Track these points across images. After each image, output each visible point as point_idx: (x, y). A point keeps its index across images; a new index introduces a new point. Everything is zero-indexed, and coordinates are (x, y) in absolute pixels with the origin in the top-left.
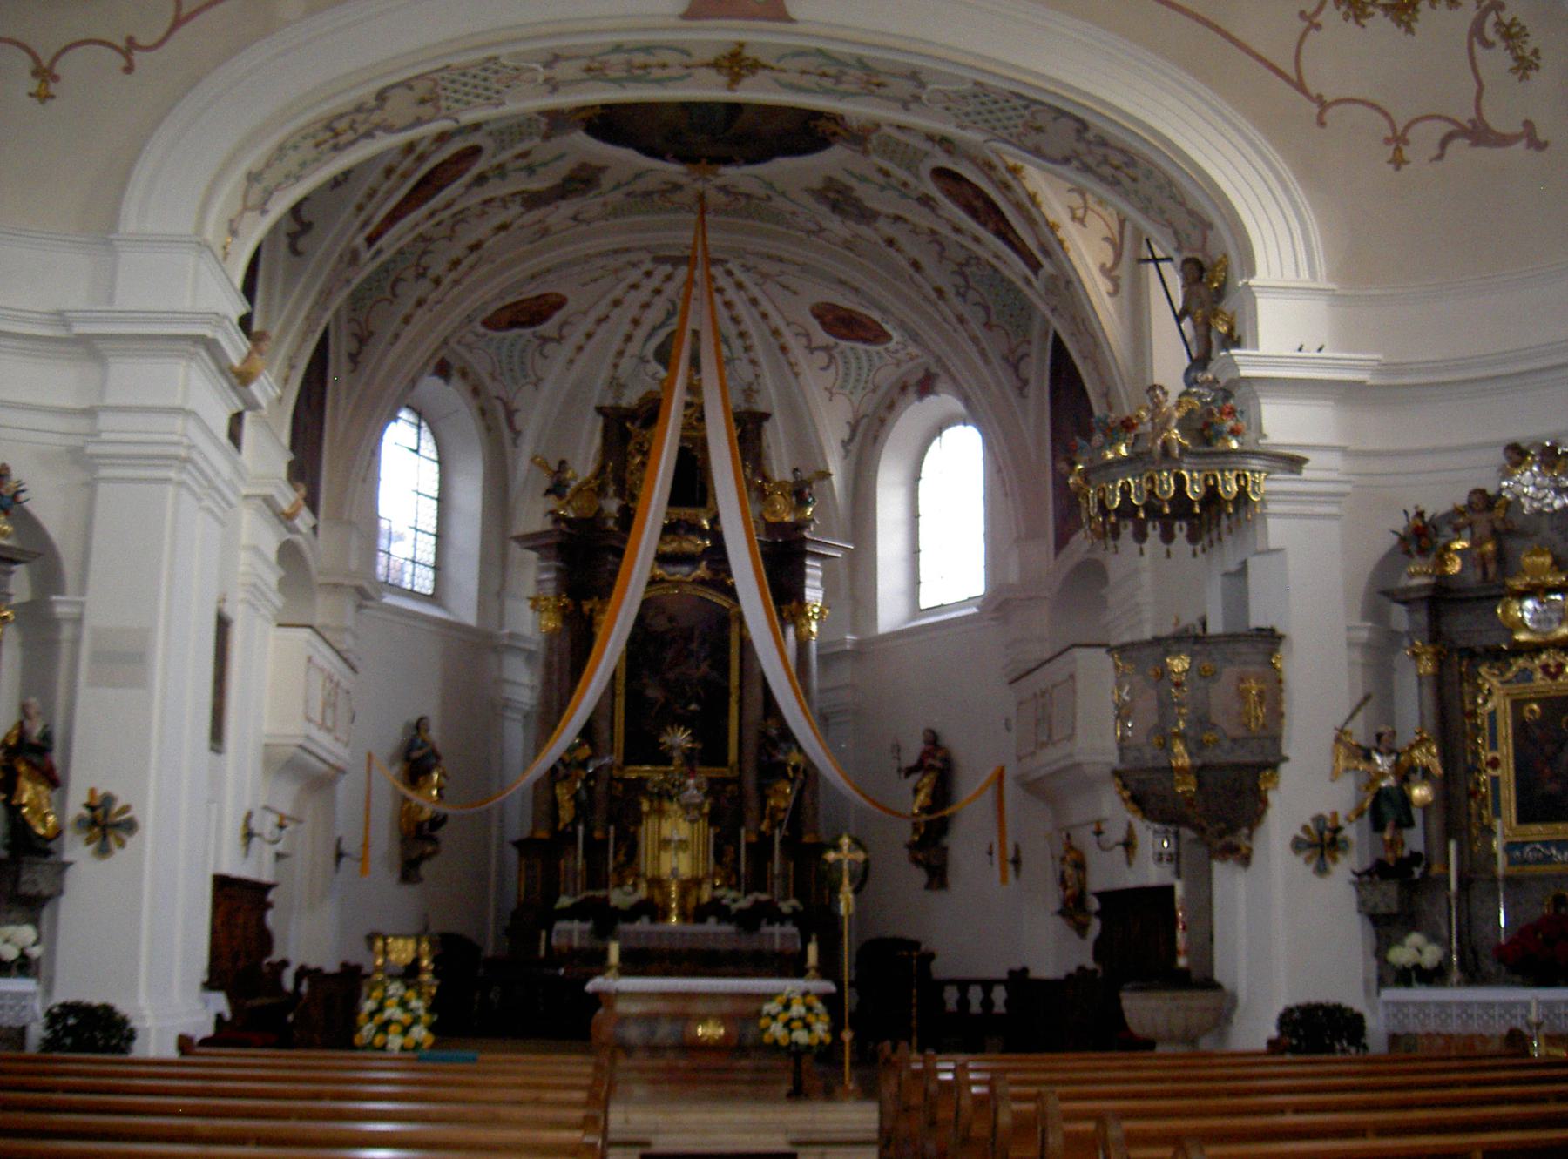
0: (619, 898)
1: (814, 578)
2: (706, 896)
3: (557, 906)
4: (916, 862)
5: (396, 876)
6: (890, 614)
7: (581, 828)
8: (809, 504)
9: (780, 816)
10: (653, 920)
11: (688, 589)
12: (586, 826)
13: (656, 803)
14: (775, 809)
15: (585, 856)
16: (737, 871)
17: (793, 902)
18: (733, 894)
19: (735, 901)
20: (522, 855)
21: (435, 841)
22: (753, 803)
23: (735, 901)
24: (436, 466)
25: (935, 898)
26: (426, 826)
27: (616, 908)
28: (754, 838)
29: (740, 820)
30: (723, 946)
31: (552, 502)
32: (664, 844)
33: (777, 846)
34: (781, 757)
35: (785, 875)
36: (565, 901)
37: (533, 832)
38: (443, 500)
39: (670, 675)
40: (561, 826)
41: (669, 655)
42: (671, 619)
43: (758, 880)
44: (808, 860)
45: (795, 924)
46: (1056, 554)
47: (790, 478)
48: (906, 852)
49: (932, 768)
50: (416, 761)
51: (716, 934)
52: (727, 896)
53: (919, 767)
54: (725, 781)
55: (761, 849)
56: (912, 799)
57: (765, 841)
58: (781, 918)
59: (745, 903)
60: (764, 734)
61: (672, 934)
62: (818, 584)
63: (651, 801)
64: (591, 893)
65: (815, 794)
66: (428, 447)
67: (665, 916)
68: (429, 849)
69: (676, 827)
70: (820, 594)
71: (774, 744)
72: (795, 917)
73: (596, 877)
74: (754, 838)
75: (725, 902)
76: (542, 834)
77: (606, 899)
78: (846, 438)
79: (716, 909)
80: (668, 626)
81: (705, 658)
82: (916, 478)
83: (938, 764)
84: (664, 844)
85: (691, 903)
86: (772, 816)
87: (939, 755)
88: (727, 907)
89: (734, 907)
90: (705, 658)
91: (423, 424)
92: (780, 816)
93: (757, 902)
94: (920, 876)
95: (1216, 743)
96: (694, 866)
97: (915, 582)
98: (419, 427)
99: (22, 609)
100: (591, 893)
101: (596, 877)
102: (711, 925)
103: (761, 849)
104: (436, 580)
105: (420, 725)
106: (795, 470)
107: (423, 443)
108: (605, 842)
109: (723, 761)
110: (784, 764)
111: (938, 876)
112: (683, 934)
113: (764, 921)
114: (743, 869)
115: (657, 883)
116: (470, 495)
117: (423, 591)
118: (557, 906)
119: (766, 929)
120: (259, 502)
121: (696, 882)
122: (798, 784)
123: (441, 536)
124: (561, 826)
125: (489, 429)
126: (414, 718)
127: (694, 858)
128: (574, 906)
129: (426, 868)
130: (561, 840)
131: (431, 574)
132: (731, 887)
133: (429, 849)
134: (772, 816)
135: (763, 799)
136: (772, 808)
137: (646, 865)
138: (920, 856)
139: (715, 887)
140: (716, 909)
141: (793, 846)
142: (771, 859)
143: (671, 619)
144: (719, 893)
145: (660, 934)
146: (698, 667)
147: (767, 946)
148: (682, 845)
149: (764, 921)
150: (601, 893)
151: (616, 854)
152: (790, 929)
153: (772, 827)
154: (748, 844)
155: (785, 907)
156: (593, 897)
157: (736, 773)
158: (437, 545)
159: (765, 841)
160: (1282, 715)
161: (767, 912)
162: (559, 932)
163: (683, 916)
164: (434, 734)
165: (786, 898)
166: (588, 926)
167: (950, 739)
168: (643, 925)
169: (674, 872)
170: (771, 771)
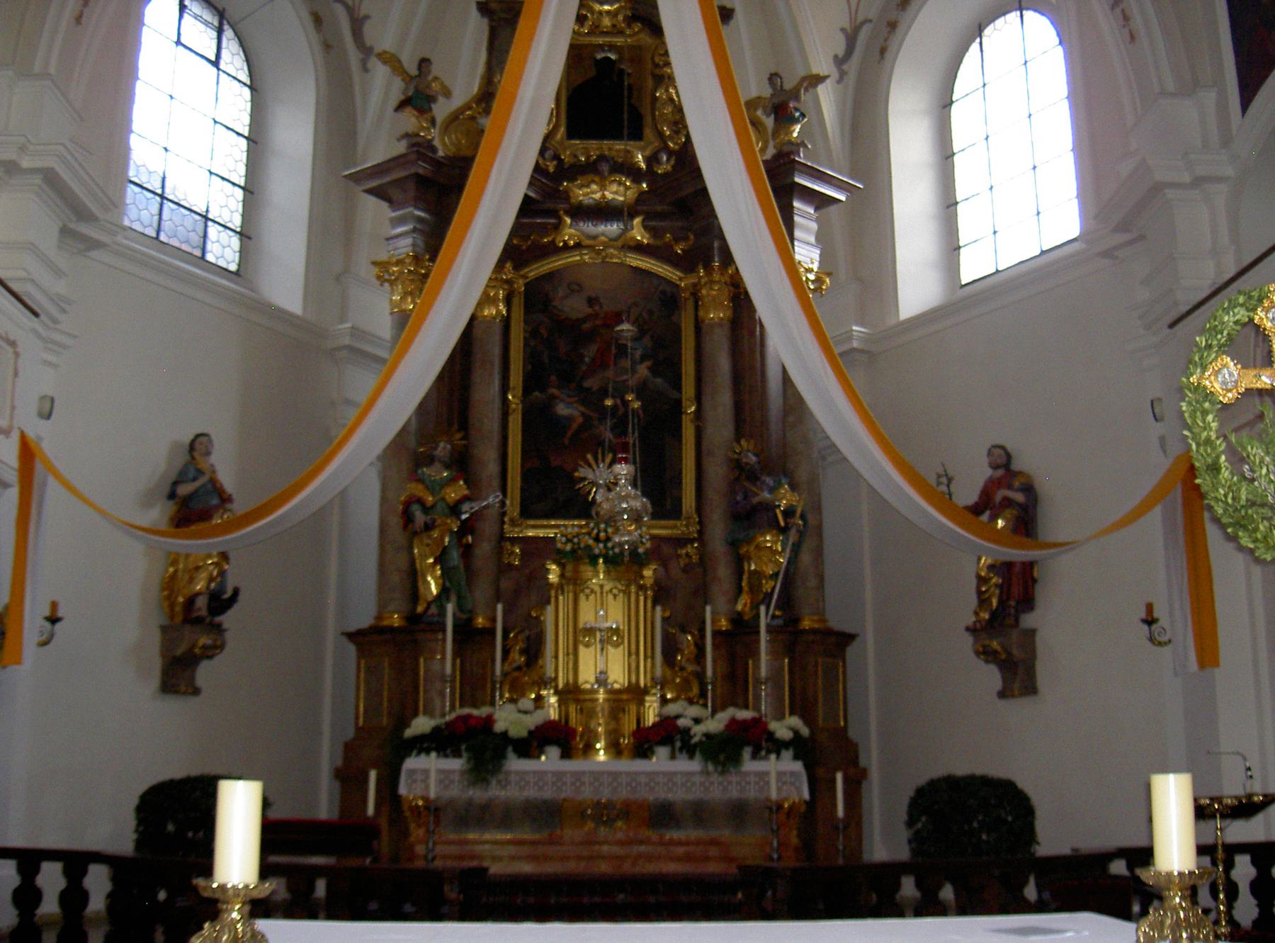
0: (510, 718)
1: (807, 230)
2: (651, 715)
3: (409, 733)
4: (987, 654)
5: (155, 681)
6: (916, 290)
7: (450, 608)
8: (795, 121)
9: (767, 586)
10: (567, 754)
11: (615, 256)
12: (460, 607)
13: (569, 567)
14: (757, 574)
15: (457, 653)
16: (700, 676)
17: (795, 721)
18: (694, 711)
19: (697, 721)
20: (362, 653)
21: (219, 629)
22: (723, 571)
23: (697, 721)
24: (247, 93)
25: (1018, 709)
26: (201, 602)
27: (504, 734)
28: (724, 624)
29: (702, 593)
30: (678, 795)
31: (409, 121)
32: (582, 634)
33: (763, 636)
34: (766, 495)
35: (775, 678)
36: (421, 725)
37: (379, 617)
38: (256, 140)
39: (592, 383)
40: (420, 609)
41: (590, 352)
42: (591, 301)
43: (736, 686)
44: (818, 651)
45: (796, 757)
46: (1246, 103)
47: (767, 92)
48: (969, 640)
49: (1008, 503)
50: (193, 501)
51: (670, 775)
52: (686, 713)
53: (985, 505)
54: (680, 542)
55: (739, 635)
56: (974, 554)
57: (742, 629)
58: (777, 746)
59: (716, 724)
60: (737, 465)
61: (597, 775)
62: (812, 239)
63: (562, 566)
64: (466, 711)
65: (819, 553)
66: (233, 60)
67: (589, 749)
68: (204, 640)
69: (605, 605)
70: (815, 254)
71: (753, 477)
72: (800, 747)
73: (474, 686)
74: (724, 624)
75: (682, 722)
76: (396, 620)
77: (489, 720)
78: (841, 53)
79: (667, 734)
80: (589, 310)
81: (644, 358)
82: (945, 103)
83: (1019, 497)
84: (582, 634)
85: (629, 725)
86: (754, 589)
87: (1017, 484)
88: (686, 732)
89: (698, 730)
90: (644, 358)
91: (226, 27)
92: (767, 586)
93: (733, 722)
94: (992, 676)
95: (558, 736)
96: (632, 669)
97: (951, 249)
98: (220, 32)
99: (1130, 867)
100: (466, 711)
101: (474, 686)
102: (660, 761)
103: (739, 635)
104: (243, 252)
105: (198, 446)
106: (773, 77)
107: (224, 53)
108: (491, 632)
109: (676, 513)
110: (770, 508)
111: (1018, 674)
112: (615, 775)
113: (747, 752)
114: (709, 673)
115: (572, 693)
116: (297, 135)
117: (222, 263)
118: (409, 733)
119: (750, 765)
120: (38, 180)
121: (636, 693)
122: (793, 536)
123: (252, 191)
124: (420, 609)
125: (327, 47)
126: (187, 438)
127: (632, 653)
128: (436, 730)
129: (205, 673)
130: (420, 625)
131: (235, 242)
132: (691, 702)
133: (204, 640)
134: (754, 589)
135: (739, 562)
136: (752, 573)
137: (554, 664)
138: (995, 645)
139: (664, 701)
140: (667, 734)
141: (790, 634)
142: (755, 653)
143: (591, 301)
144: (672, 709)
145: (578, 775)
146: (634, 371)
147: (752, 793)
148: (610, 637)
149: (747, 752)
150: (483, 711)
151: (506, 652)
152: (788, 764)
153: (755, 607)
154: (716, 633)
155: (782, 729)
156: (469, 716)
157: (693, 530)
158: (245, 202)
159: (742, 629)
160: (1034, 581)
161: (751, 737)
162: (412, 772)
163: (615, 748)
164: (225, 467)
165: (780, 717)
166: (455, 764)
167: (1024, 462)
168: (549, 760)
169: (602, 680)
170: (750, 517)
